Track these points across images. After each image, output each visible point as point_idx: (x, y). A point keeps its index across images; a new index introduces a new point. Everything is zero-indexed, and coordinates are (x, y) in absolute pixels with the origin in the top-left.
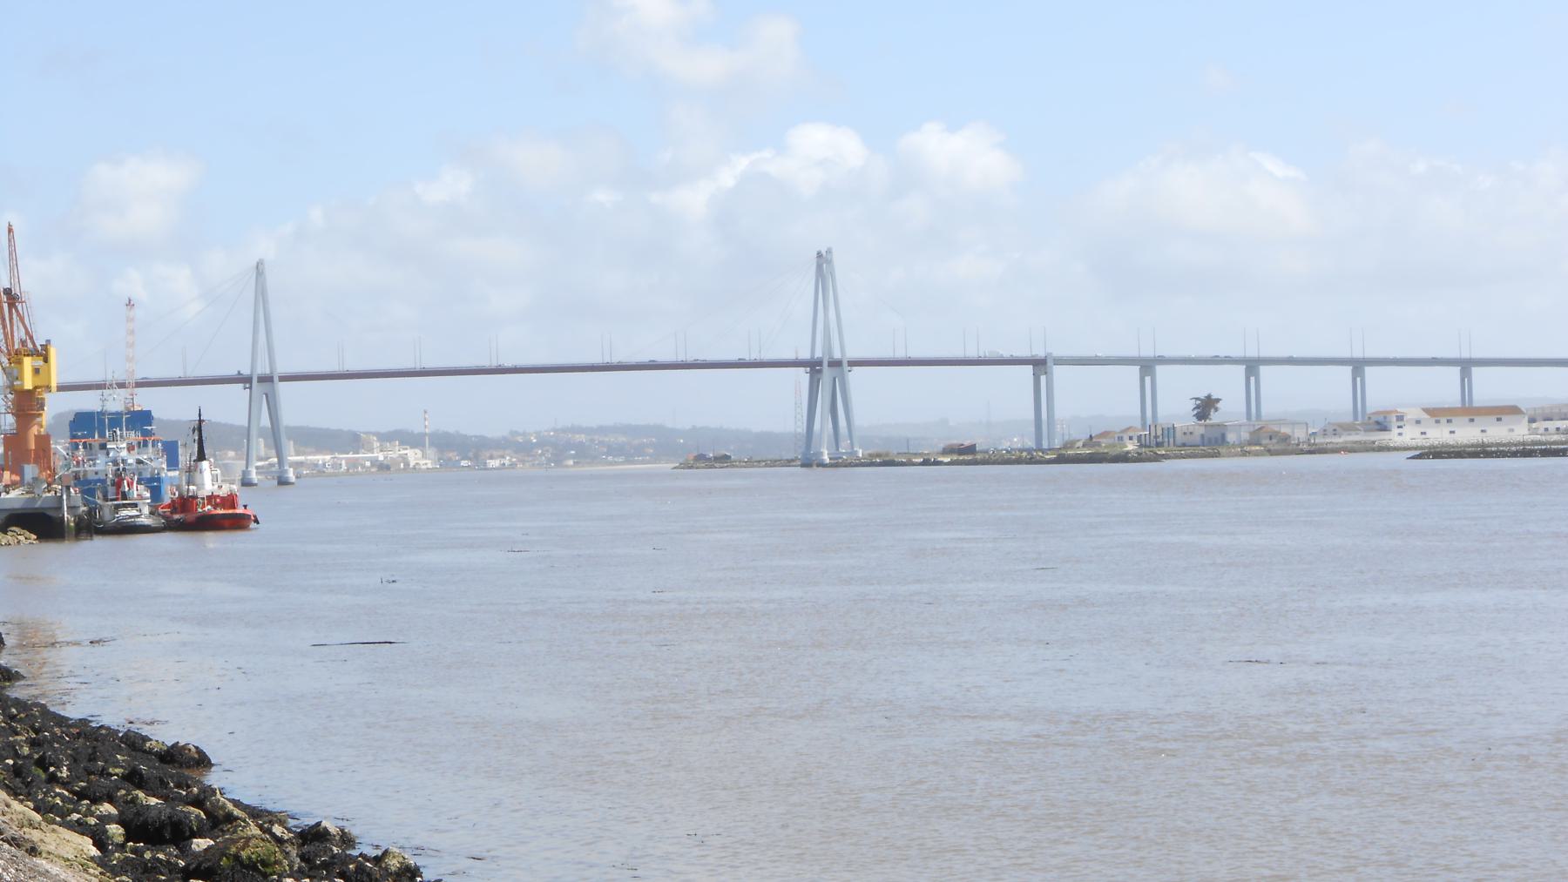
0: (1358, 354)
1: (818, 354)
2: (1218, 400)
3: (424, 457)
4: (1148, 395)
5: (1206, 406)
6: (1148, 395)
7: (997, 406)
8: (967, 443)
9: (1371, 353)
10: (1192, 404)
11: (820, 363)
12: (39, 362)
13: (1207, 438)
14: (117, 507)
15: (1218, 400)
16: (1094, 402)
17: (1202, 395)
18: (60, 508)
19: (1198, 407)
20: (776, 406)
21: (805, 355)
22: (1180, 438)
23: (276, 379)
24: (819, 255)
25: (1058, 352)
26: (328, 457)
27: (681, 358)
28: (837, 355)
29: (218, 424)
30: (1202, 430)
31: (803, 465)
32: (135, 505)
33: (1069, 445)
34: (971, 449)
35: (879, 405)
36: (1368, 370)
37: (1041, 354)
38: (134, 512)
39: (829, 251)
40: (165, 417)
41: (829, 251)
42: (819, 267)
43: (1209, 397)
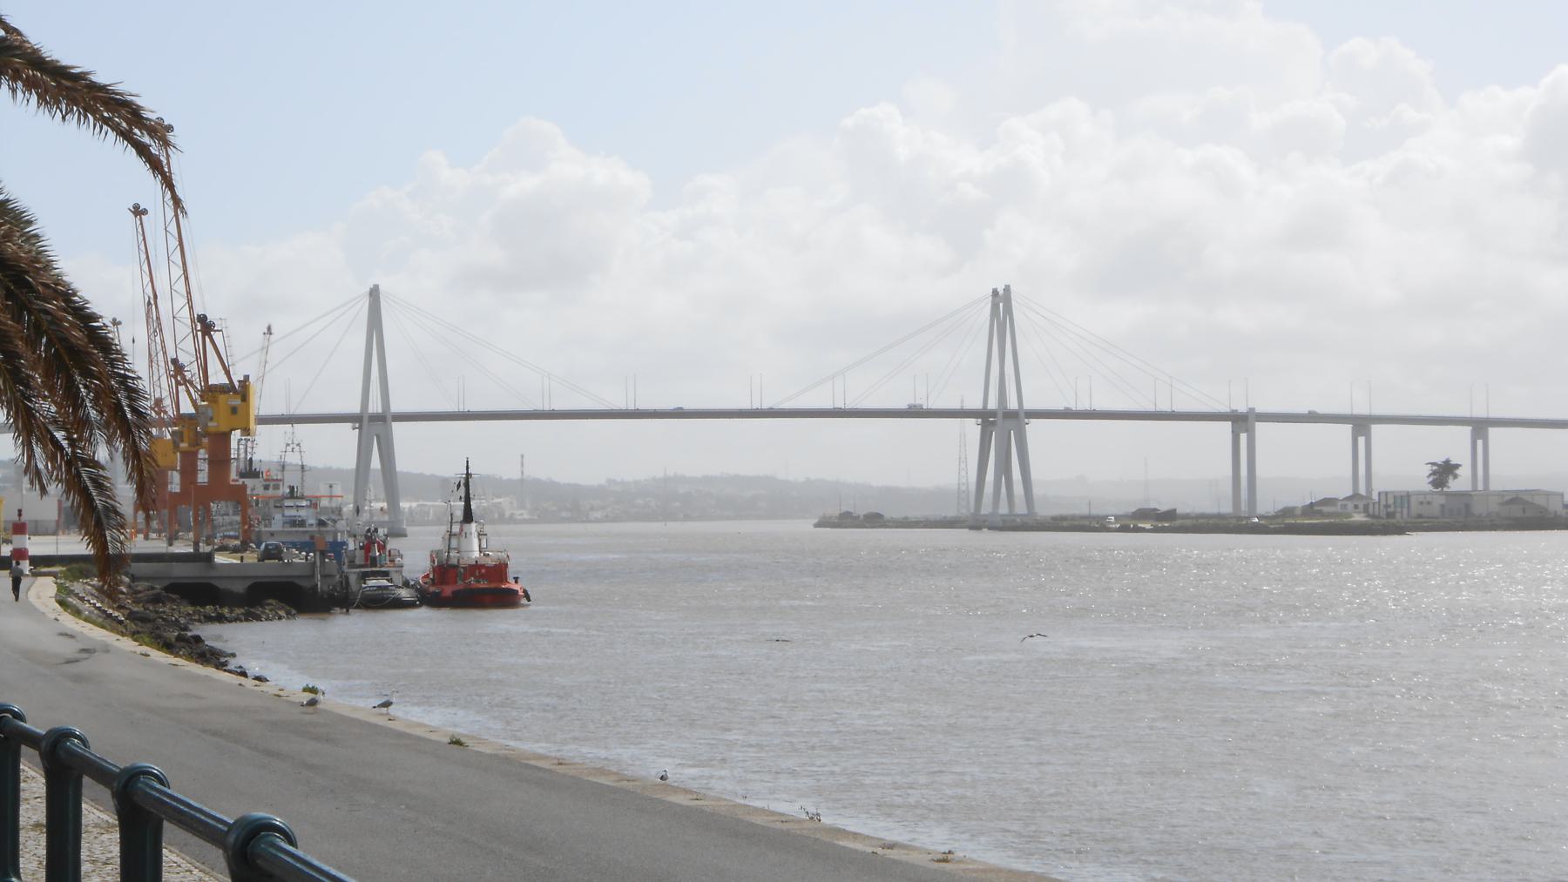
0: (1480, 413)
1: (992, 404)
2: (1457, 466)
3: (522, 507)
4: (1362, 458)
5: (1444, 471)
6: (1362, 458)
7: (1194, 466)
8: (1163, 508)
9: (1495, 413)
10: (1428, 470)
11: (993, 413)
12: (237, 402)
13: (1451, 508)
14: (364, 577)
15: (1457, 466)
16: (1302, 465)
17: (1440, 460)
18: (313, 576)
19: (1434, 473)
20: (942, 460)
21: (977, 404)
22: (1415, 508)
23: (389, 418)
24: (995, 293)
25: (1261, 408)
26: (414, 505)
27: (1150, 408)
28: (1013, 404)
29: (408, 474)
30: (1442, 500)
31: (971, 528)
32: (385, 574)
33: (1287, 512)
34: (1171, 515)
35: (1061, 463)
36: (1493, 432)
37: (1242, 408)
38: (384, 582)
39: (1007, 289)
40: (320, 465)
41: (1007, 289)
42: (995, 307)
43: (1447, 462)
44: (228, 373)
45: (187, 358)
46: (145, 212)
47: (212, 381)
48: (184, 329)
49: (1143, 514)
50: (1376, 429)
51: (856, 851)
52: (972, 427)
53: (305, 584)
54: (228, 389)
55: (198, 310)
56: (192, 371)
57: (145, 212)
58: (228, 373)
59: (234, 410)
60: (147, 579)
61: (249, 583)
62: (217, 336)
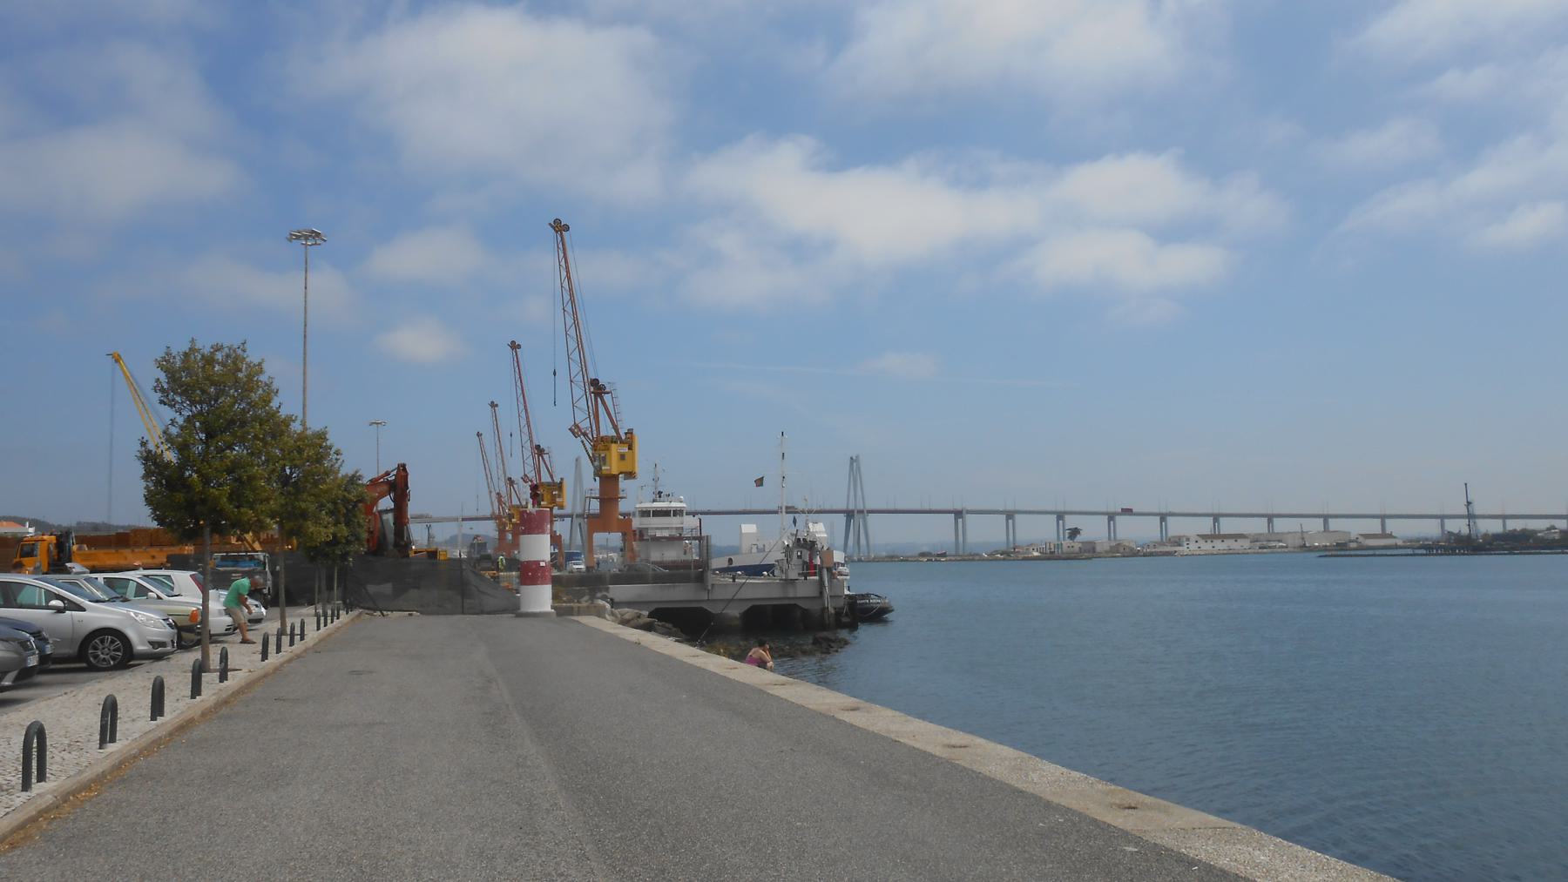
1: (851, 507)
12: (625, 449)
16: (986, 533)
21: (843, 507)
44: (615, 427)
45: (503, 492)
46: (567, 228)
47: (603, 434)
48: (502, 484)
49: (923, 555)
50: (1017, 517)
51: (669, 658)
52: (842, 518)
53: (814, 607)
54: (616, 440)
55: (536, 442)
56: (505, 499)
57: (567, 228)
58: (615, 427)
59: (622, 457)
60: (629, 604)
61: (750, 605)
62: (607, 397)
